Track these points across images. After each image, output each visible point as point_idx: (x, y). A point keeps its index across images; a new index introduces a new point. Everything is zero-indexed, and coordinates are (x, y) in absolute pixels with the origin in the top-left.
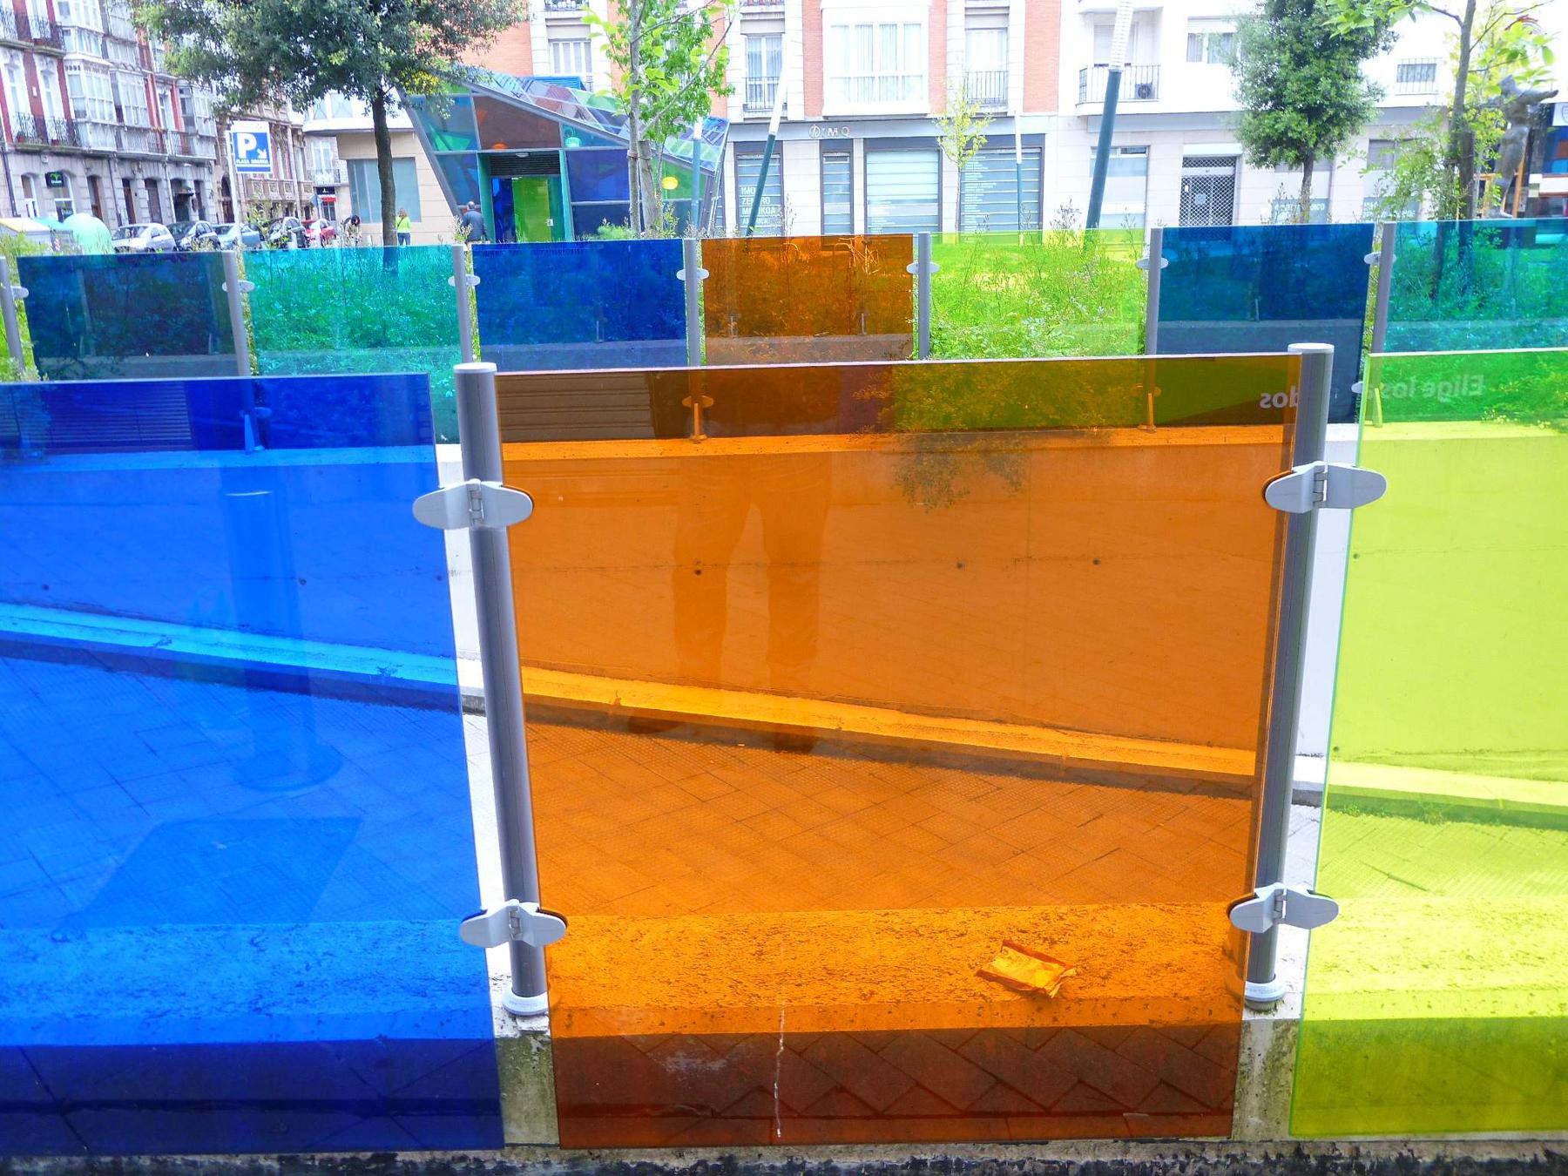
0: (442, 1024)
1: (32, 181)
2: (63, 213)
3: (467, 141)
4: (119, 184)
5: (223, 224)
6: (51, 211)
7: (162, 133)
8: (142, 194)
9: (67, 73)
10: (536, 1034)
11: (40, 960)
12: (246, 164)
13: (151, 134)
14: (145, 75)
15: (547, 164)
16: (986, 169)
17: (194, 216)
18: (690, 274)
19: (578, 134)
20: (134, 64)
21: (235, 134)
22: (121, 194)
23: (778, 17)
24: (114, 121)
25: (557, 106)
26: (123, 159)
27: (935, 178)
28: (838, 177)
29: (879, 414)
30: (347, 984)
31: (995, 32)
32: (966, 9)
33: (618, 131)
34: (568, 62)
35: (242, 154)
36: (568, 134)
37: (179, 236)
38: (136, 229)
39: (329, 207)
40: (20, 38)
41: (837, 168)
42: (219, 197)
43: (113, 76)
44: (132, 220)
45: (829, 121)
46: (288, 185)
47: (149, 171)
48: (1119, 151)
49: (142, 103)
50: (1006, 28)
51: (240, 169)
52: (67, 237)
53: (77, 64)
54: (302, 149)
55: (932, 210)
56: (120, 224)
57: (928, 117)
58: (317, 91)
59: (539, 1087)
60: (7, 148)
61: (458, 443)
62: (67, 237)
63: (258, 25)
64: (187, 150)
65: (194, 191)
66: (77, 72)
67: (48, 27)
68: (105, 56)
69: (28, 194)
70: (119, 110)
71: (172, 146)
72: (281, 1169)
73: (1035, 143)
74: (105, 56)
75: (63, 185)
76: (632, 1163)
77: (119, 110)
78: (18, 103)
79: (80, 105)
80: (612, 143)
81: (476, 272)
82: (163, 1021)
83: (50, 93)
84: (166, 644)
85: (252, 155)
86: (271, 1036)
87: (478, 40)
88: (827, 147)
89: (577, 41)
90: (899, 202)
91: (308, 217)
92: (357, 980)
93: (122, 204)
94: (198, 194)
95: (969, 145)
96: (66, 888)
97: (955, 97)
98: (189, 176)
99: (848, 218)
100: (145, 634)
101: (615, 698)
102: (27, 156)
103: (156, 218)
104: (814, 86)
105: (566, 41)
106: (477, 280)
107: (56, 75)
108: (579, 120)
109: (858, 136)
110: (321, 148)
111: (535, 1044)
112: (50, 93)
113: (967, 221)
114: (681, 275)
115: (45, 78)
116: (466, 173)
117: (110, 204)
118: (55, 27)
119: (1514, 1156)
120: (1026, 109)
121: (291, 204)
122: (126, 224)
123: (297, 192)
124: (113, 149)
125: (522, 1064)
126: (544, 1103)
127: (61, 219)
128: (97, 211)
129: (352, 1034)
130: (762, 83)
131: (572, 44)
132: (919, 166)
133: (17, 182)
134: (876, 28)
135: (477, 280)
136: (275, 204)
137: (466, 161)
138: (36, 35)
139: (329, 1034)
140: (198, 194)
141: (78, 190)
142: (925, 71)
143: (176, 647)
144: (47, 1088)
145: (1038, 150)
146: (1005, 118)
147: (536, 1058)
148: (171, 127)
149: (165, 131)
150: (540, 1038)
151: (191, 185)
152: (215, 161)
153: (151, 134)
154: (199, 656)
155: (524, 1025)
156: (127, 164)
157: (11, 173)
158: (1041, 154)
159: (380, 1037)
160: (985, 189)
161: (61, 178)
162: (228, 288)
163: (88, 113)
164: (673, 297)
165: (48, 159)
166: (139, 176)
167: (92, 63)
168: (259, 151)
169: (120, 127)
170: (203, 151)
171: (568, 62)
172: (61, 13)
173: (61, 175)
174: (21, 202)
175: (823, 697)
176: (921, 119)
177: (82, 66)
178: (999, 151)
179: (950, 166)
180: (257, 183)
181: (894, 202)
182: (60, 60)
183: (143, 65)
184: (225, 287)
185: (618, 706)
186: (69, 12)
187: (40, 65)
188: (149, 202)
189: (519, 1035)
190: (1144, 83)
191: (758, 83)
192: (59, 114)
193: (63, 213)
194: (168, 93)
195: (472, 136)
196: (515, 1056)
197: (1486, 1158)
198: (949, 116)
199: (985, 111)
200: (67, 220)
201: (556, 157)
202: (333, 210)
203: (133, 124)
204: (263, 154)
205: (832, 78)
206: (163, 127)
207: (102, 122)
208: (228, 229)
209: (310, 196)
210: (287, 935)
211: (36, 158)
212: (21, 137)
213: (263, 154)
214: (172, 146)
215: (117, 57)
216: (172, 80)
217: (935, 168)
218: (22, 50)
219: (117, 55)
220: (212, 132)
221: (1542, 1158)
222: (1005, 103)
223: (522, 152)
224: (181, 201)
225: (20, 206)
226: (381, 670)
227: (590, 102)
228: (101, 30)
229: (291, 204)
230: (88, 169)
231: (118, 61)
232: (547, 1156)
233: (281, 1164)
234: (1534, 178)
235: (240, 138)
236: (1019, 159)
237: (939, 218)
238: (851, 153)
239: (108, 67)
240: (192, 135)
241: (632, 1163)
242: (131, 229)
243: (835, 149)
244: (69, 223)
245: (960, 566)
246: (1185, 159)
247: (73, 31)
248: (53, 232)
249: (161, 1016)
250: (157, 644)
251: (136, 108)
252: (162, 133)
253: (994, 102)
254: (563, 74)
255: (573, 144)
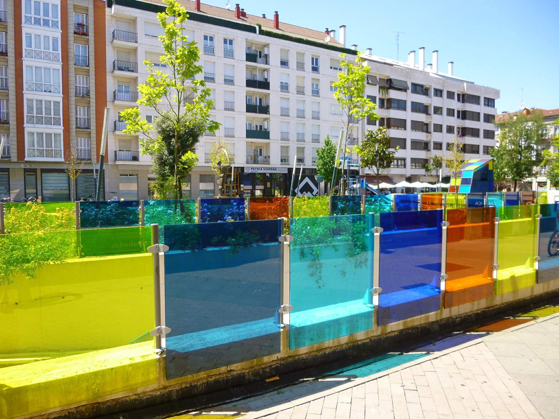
16: (85, 179)
55: (67, 192)
61: (470, 192)
86: (46, 385)
99: (68, 191)
119: (60, 415)
132: (62, 177)
144: (347, 335)
190: (135, 156)
197: (53, 417)
221: (67, 414)
234: (242, 186)
237: (69, 194)
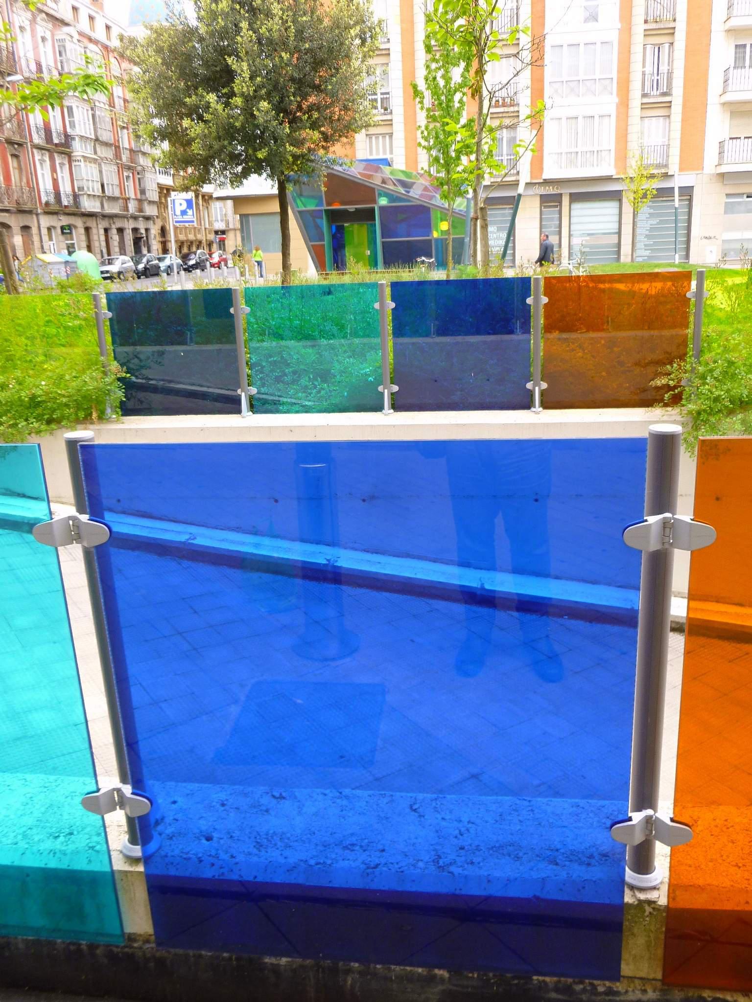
0: (579, 890)
1: (53, 230)
2: (71, 250)
3: (315, 202)
4: (102, 232)
5: (161, 256)
6: (63, 249)
7: (127, 200)
8: (115, 237)
9: (74, 164)
10: (650, 902)
11: (272, 813)
12: (180, 218)
13: (121, 201)
14: (118, 164)
15: (367, 215)
17: (144, 251)
18: (537, 300)
19: (386, 195)
20: (112, 158)
21: (174, 200)
22: (103, 238)
23: (515, 114)
24: (100, 193)
25: (370, 176)
26: (104, 216)
27: (616, 218)
28: (552, 219)
29: (666, 395)
30: (497, 849)
31: (662, 118)
32: (642, 104)
33: (408, 192)
34: (377, 149)
35: (178, 213)
36: (380, 195)
37: (137, 263)
38: (112, 259)
39: (222, 244)
40: (47, 143)
41: (551, 213)
42: (159, 238)
43: (100, 165)
44: (109, 254)
45: (547, 182)
46: (199, 230)
47: (119, 224)
48: (745, 196)
49: (116, 181)
50: (669, 116)
51: (177, 222)
52: (73, 265)
53: (79, 158)
54: (207, 208)
56: (102, 257)
57: (614, 177)
58: (245, 174)
59: (647, 939)
60: (39, 211)
62: (73, 265)
63: (214, 134)
64: (141, 210)
65: (144, 235)
66: (79, 163)
67: (63, 136)
68: (95, 153)
69: (51, 239)
70: (103, 186)
71: (132, 207)
72: (449, 978)
73: (687, 192)
74: (95, 153)
75: (71, 233)
76: (709, 997)
77: (103, 186)
78: (45, 184)
79: (81, 184)
80: (409, 201)
81: (392, 300)
82: (377, 870)
83: (63, 175)
84: (193, 539)
85: (184, 213)
87: (344, 140)
88: (545, 200)
89: (384, 135)
90: (592, 234)
91: (210, 250)
92: (501, 847)
93: (104, 244)
94: (147, 237)
95: (645, 196)
96: (163, 705)
97: (633, 164)
98: (141, 225)
100: (179, 533)
101: (480, 583)
102: (50, 216)
103: (123, 252)
104: (538, 163)
105: (377, 135)
106: (393, 305)
107: (67, 166)
108: (384, 185)
109: (566, 191)
110: (218, 206)
111: (648, 909)
112: (63, 175)
113: (639, 245)
114: (529, 301)
115: (61, 167)
116: (314, 221)
117: (96, 244)
118: (67, 136)
120: (681, 169)
121: (200, 242)
122: (106, 257)
123: (204, 234)
124: (99, 210)
125: (636, 922)
126: (649, 950)
127: (70, 253)
128: (89, 249)
129: (513, 892)
130: (503, 158)
131: (381, 137)
133: (44, 232)
134: (580, 119)
135: (393, 305)
136: (192, 242)
137: (315, 214)
138: (56, 141)
139: (496, 891)
140: (147, 237)
141: (79, 236)
142: (612, 147)
143: (199, 541)
145: (689, 197)
146: (666, 176)
147: (647, 919)
148: (132, 196)
149: (129, 199)
150: (653, 906)
151: (143, 231)
152: (157, 217)
153: (121, 201)
154: (214, 548)
155: (642, 896)
156: (106, 219)
157: (41, 226)
158: (690, 200)
159: (535, 896)
160: (651, 225)
161: (70, 229)
162: (235, 310)
163: (85, 189)
164: (525, 314)
165: (62, 217)
166: (113, 226)
167: (88, 157)
168: (188, 210)
169: (104, 197)
170: (151, 211)
171: (377, 149)
172: (70, 127)
173: (70, 227)
174: (47, 244)
175: (619, 584)
176: (609, 179)
177: (82, 160)
178: (661, 199)
179: (627, 209)
180: (181, 229)
181: (589, 235)
182: (69, 156)
183: (117, 158)
184: (232, 310)
185: (483, 588)
186: (74, 126)
187: (58, 160)
188: (119, 243)
189: (636, 903)
191: (500, 158)
192: (69, 189)
193: (71, 250)
194: (131, 175)
195: (320, 198)
196: (632, 916)
198: (631, 176)
199: (655, 172)
200: (74, 255)
201: (372, 211)
202: (224, 245)
203: (110, 195)
204: (190, 212)
205: (549, 154)
206: (127, 196)
207: (93, 193)
208: (165, 258)
209: (211, 237)
210: (434, 804)
211: (55, 217)
212: (47, 204)
213: (190, 212)
214: (132, 207)
215: (102, 154)
216: (133, 167)
217: (617, 211)
218: (48, 150)
219: (104, 152)
220: (156, 198)
222: (666, 166)
223: (351, 208)
224: (137, 241)
225: (46, 247)
226: (328, 560)
227: (391, 173)
228: (93, 137)
229: (200, 242)
230: (85, 223)
231: (102, 156)
232: (644, 985)
233: (450, 974)
235: (177, 203)
236: (677, 204)
237: (619, 245)
238: (560, 202)
239: (97, 160)
240: (144, 200)
241: (709, 997)
242: (109, 260)
243: (550, 201)
244: (74, 257)
245: (718, 499)
246: (726, 195)
247: (77, 138)
248: (67, 263)
249: (375, 868)
250: (188, 539)
251: (112, 185)
252: (127, 200)
253: (658, 166)
254: (374, 157)
255: (383, 201)
